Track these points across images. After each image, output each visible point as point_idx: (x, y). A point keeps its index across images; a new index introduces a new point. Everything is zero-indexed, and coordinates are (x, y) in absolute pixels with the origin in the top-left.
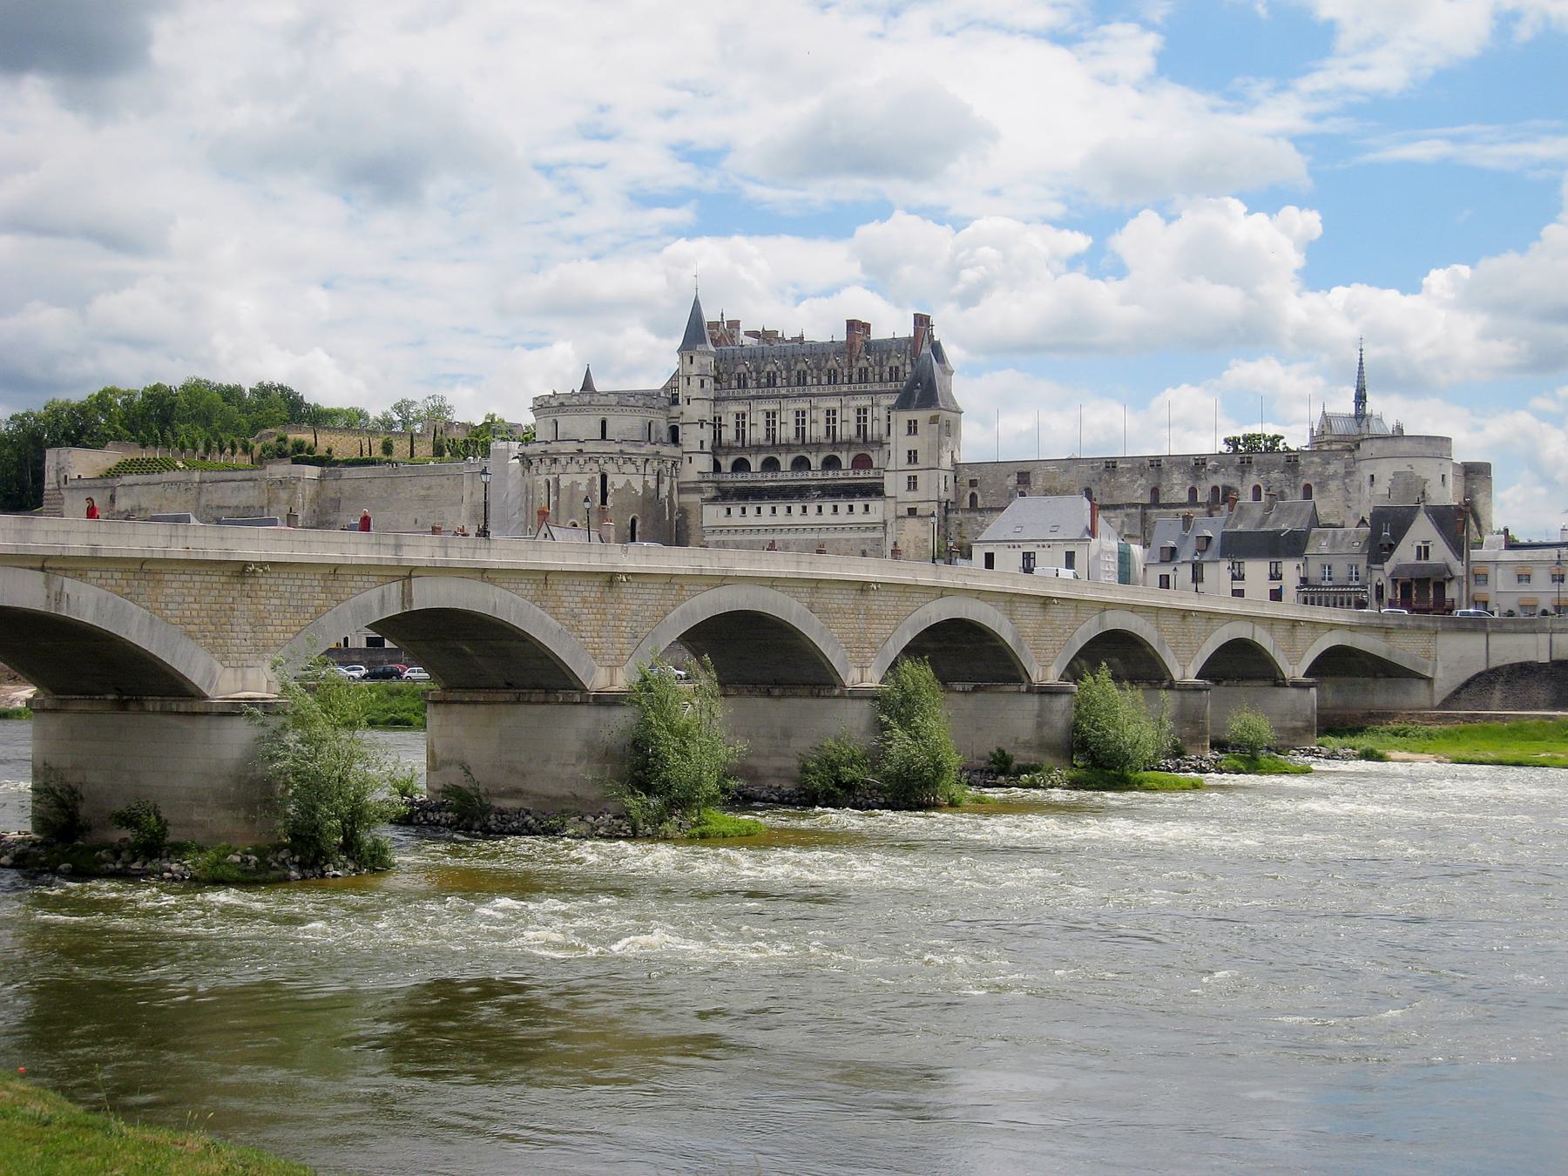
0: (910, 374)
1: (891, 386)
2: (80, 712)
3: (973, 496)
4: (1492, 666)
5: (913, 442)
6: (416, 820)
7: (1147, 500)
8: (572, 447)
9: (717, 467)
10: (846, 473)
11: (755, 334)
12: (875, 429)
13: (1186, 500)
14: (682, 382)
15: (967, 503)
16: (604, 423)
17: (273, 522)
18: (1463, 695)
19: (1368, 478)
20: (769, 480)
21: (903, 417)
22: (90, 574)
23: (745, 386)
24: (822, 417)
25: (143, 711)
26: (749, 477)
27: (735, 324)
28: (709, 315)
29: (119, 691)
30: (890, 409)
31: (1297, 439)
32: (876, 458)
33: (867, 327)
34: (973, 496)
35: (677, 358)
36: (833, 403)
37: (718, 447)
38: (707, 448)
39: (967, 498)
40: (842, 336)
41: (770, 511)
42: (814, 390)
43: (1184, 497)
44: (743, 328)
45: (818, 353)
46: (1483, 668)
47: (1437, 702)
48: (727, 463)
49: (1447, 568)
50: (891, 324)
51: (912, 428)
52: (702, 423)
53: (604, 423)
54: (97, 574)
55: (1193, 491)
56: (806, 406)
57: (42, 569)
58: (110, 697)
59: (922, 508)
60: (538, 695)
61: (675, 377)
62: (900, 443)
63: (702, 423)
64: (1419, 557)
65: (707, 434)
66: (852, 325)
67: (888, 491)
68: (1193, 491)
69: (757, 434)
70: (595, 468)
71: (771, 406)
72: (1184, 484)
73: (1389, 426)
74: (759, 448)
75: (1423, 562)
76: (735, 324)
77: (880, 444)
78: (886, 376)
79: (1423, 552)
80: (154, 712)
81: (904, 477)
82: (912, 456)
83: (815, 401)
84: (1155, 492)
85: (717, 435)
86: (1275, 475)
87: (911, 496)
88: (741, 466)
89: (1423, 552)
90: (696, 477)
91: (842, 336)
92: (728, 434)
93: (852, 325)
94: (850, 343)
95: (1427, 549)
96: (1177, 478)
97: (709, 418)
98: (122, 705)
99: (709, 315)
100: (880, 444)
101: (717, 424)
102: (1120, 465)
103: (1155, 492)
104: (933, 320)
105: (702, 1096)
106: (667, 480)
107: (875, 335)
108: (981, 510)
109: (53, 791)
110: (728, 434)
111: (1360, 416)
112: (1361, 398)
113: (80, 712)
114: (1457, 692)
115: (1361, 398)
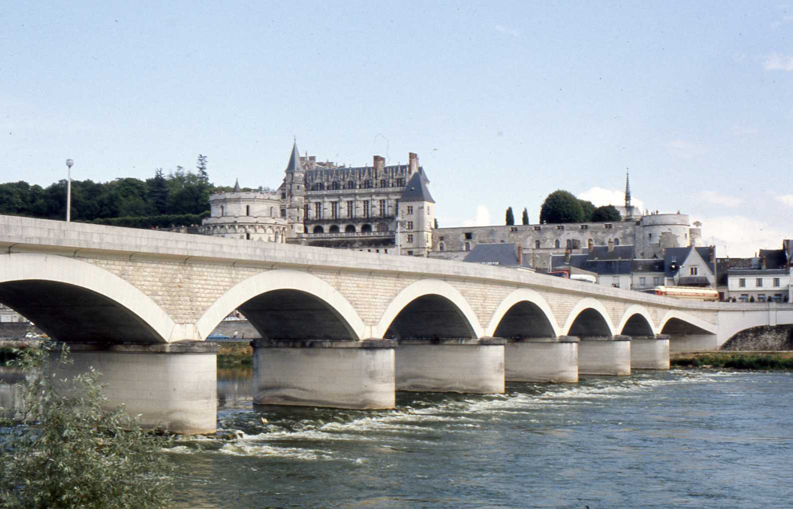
0: (412, 187)
8: (232, 220)
9: (306, 231)
13: (554, 246)
16: (248, 207)
17: (422, 255)
19: (648, 236)
20: (334, 237)
21: (403, 207)
26: (323, 235)
27: (313, 158)
33: (383, 159)
37: (307, 221)
39: (439, 247)
41: (384, 251)
44: (317, 160)
49: (706, 279)
50: (396, 158)
51: (410, 210)
53: (248, 207)
55: (557, 242)
56: (369, 198)
60: (327, 344)
64: (692, 273)
66: (377, 159)
68: (557, 242)
70: (243, 230)
74: (328, 221)
75: (694, 276)
79: (694, 271)
85: (306, 214)
86: (599, 234)
88: (318, 230)
89: (694, 271)
90: (295, 236)
91: (371, 164)
92: (312, 214)
93: (377, 159)
94: (375, 168)
95: (696, 269)
104: (419, 156)
105: (578, 446)
106: (280, 236)
107: (388, 164)
110: (312, 214)
112: (628, 198)
114: (735, 338)
115: (628, 198)
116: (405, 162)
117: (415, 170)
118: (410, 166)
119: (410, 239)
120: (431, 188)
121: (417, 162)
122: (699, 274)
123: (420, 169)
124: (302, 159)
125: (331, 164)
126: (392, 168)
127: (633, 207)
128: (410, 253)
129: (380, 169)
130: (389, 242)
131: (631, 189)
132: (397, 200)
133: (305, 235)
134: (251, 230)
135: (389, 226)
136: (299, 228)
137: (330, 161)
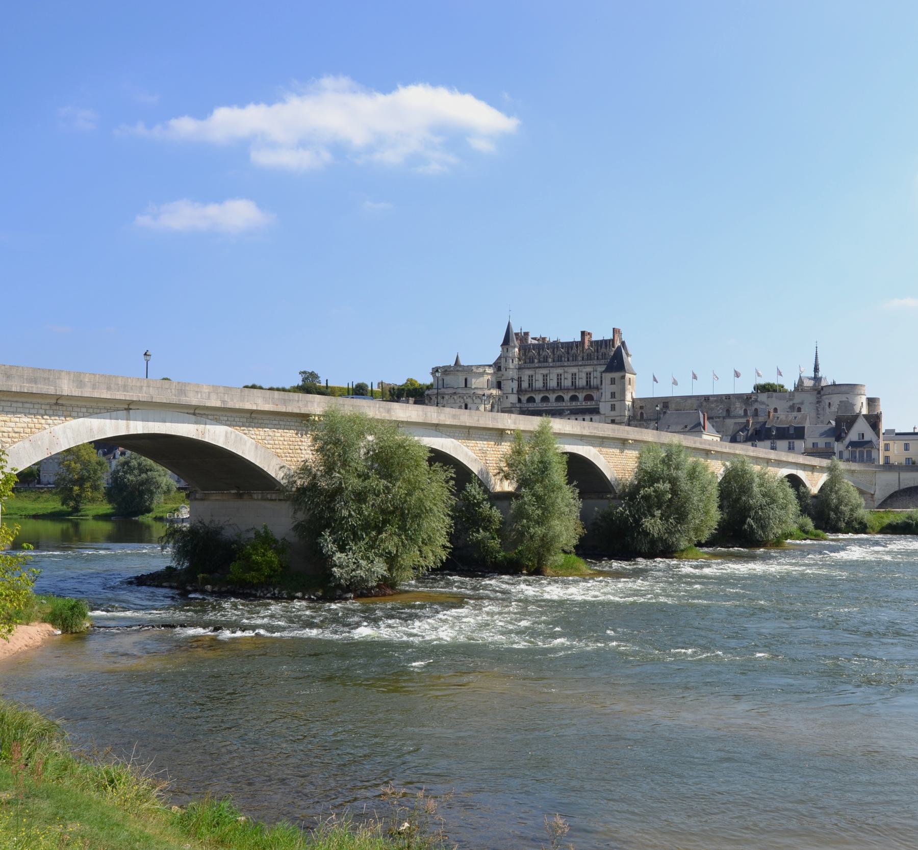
0: (611, 358)
1: (603, 361)
2: (217, 500)
3: (642, 414)
4: (902, 488)
5: (613, 388)
6: (390, 570)
7: (724, 415)
8: (451, 391)
9: (520, 400)
10: (582, 404)
11: (534, 339)
12: (595, 382)
14: (503, 360)
15: (639, 417)
16: (466, 380)
18: (889, 502)
20: (544, 406)
21: (609, 376)
22: (222, 418)
23: (533, 362)
24: (570, 377)
25: (252, 499)
27: (527, 334)
28: (515, 329)
29: (238, 488)
30: (601, 373)
31: (790, 387)
32: (595, 395)
34: (642, 414)
35: (500, 349)
36: (575, 370)
37: (520, 391)
38: (515, 391)
40: (579, 339)
42: (566, 364)
43: (742, 412)
44: (531, 335)
45: (569, 346)
46: (897, 489)
47: (877, 504)
48: (524, 398)
51: (613, 381)
52: (512, 379)
53: (466, 380)
54: (226, 418)
55: (745, 411)
57: (194, 414)
58: (233, 492)
59: (617, 419)
61: (500, 358)
62: (607, 388)
63: (512, 379)
65: (515, 385)
67: (602, 411)
69: (539, 384)
71: (545, 371)
72: (741, 408)
73: (830, 382)
76: (527, 334)
77: (597, 388)
78: (600, 357)
80: (257, 499)
81: (609, 405)
82: (613, 395)
83: (566, 369)
84: (728, 411)
85: (520, 386)
87: (613, 413)
90: (509, 405)
92: (525, 385)
96: (738, 405)
97: (516, 377)
98: (239, 496)
99: (515, 329)
100: (597, 388)
101: (520, 380)
102: (711, 399)
103: (728, 411)
104: (622, 331)
107: (595, 338)
108: (645, 421)
109: (310, 471)
110: (525, 385)
111: (817, 379)
112: (816, 369)
113: (217, 500)
114: (892, 496)
116: (609, 336)
117: (618, 344)
118: (613, 340)
119: (613, 408)
120: (630, 361)
121: (273, 145)
122: (866, 438)
123: (623, 343)
124: (517, 334)
125: (544, 339)
126: (597, 342)
127: (821, 378)
128: (613, 422)
129: (587, 344)
130: (595, 411)
131: (820, 361)
132: (601, 373)
133: (518, 405)
134: (469, 401)
135: (69, 826)
136: (513, 399)
137: (829, 377)
